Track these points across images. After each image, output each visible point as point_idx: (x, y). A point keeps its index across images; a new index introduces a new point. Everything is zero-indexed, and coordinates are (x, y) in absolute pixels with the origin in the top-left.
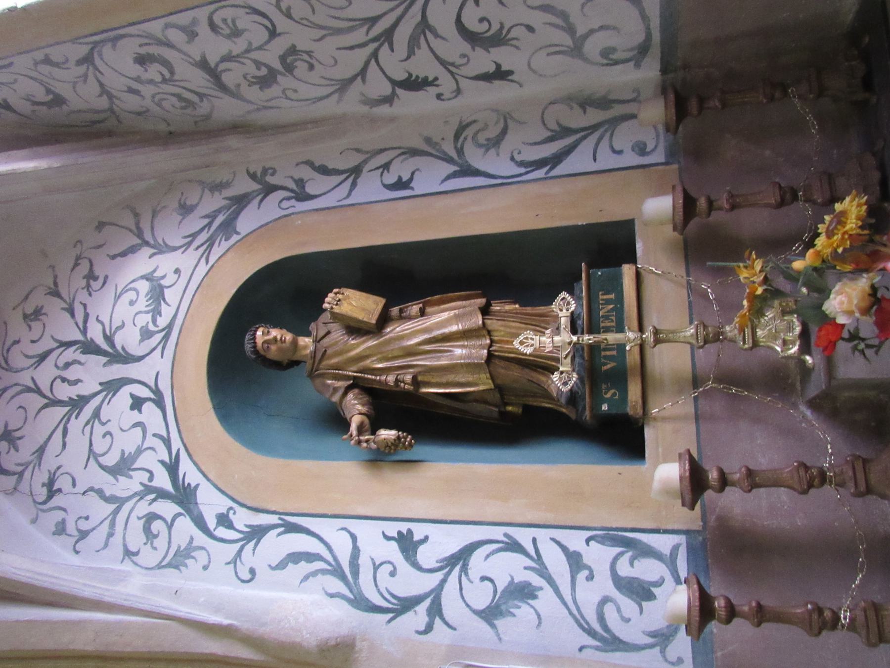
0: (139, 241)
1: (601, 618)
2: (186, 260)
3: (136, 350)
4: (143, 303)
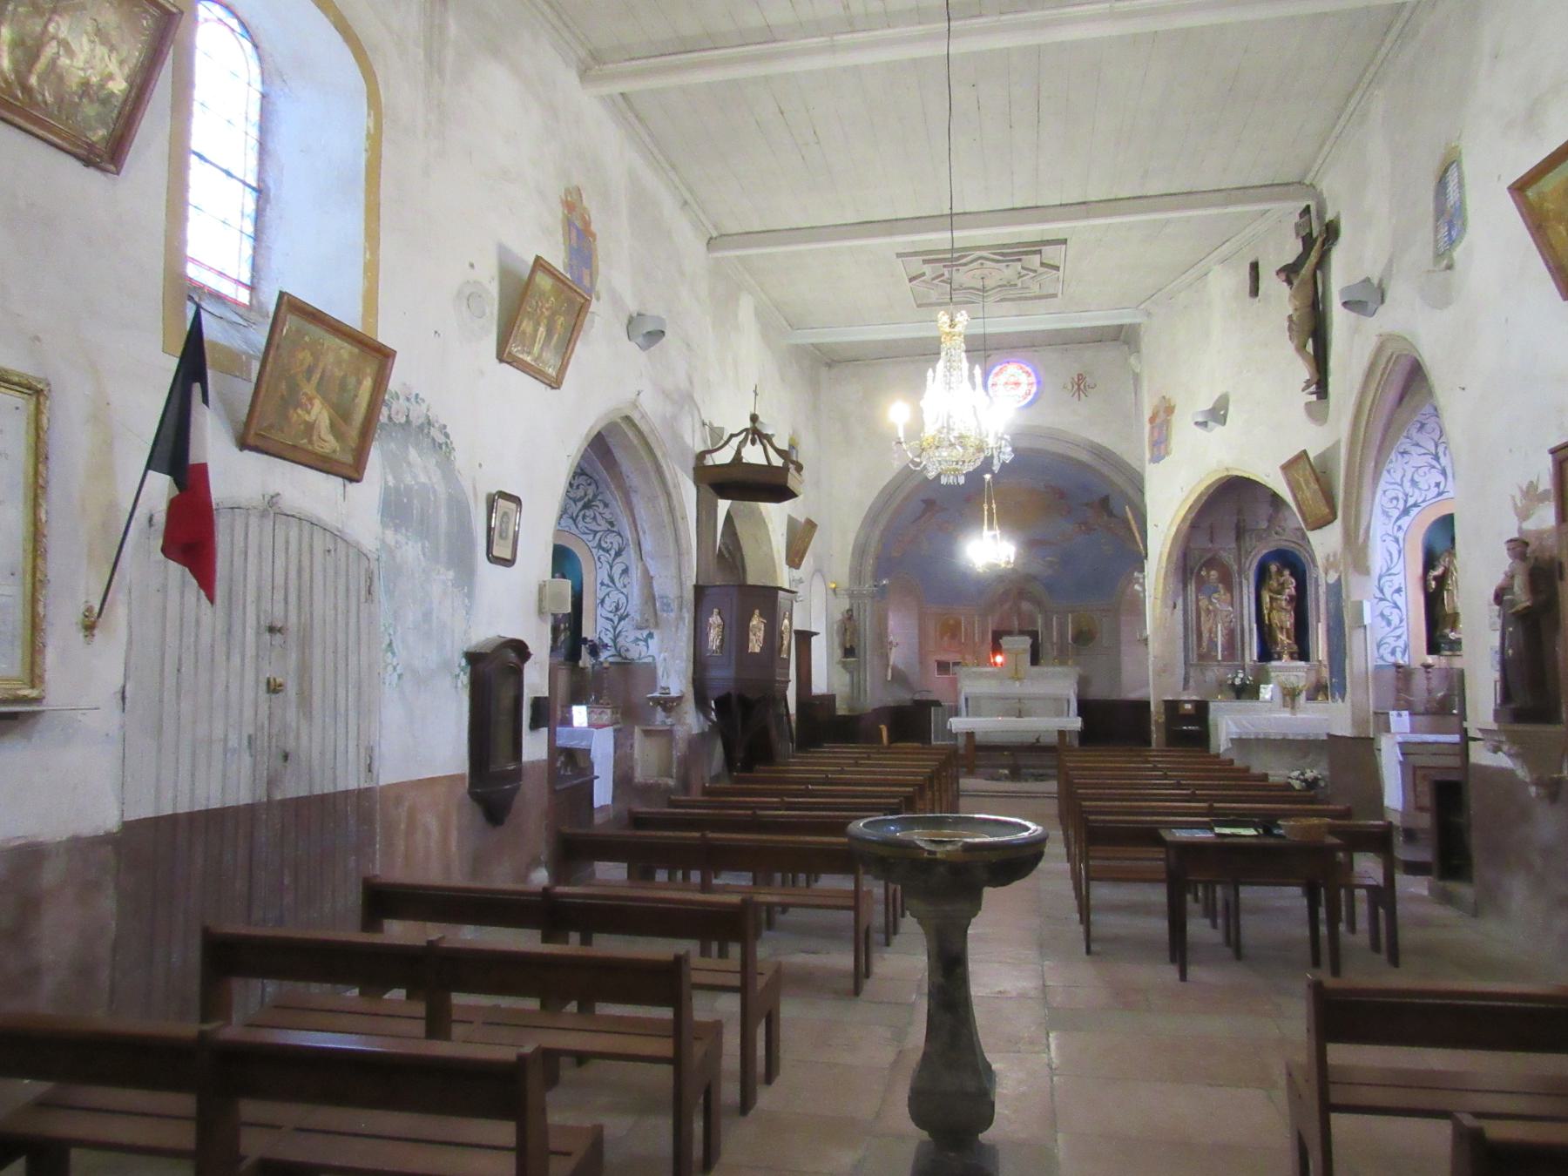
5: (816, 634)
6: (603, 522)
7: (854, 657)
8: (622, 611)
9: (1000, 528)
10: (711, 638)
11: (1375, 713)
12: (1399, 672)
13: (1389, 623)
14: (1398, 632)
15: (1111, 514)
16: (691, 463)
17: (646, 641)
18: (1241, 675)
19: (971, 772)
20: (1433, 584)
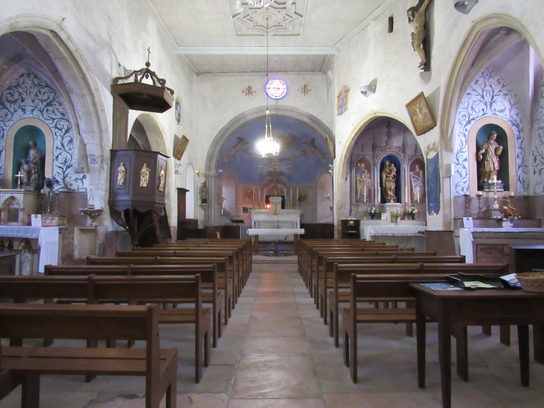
0: (512, 105)
1: (459, 185)
2: (508, 117)
3: (493, 107)
4: (501, 108)
5: (188, 191)
6: (58, 114)
7: (206, 203)
8: (68, 163)
9: (273, 137)
10: (119, 179)
11: (454, 219)
12: (467, 199)
13: (461, 176)
14: (465, 180)
15: (315, 147)
16: (110, 83)
17: (82, 180)
18: (374, 209)
19: (257, 253)
20: (481, 157)
